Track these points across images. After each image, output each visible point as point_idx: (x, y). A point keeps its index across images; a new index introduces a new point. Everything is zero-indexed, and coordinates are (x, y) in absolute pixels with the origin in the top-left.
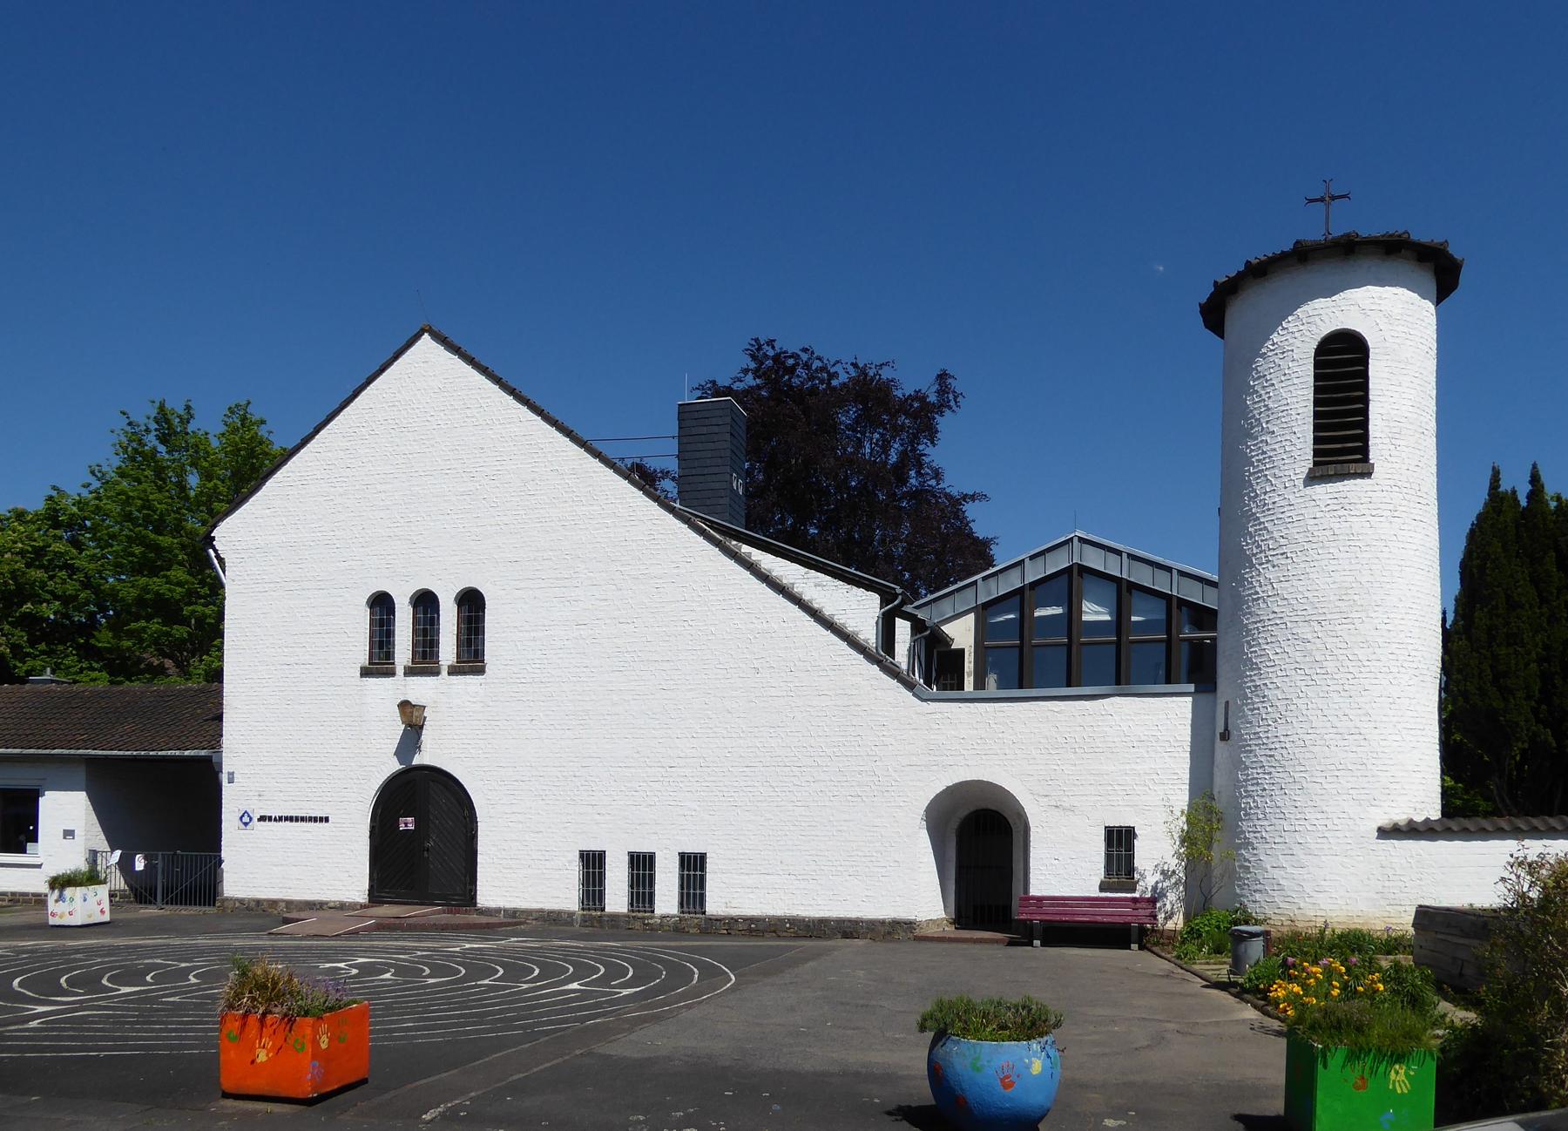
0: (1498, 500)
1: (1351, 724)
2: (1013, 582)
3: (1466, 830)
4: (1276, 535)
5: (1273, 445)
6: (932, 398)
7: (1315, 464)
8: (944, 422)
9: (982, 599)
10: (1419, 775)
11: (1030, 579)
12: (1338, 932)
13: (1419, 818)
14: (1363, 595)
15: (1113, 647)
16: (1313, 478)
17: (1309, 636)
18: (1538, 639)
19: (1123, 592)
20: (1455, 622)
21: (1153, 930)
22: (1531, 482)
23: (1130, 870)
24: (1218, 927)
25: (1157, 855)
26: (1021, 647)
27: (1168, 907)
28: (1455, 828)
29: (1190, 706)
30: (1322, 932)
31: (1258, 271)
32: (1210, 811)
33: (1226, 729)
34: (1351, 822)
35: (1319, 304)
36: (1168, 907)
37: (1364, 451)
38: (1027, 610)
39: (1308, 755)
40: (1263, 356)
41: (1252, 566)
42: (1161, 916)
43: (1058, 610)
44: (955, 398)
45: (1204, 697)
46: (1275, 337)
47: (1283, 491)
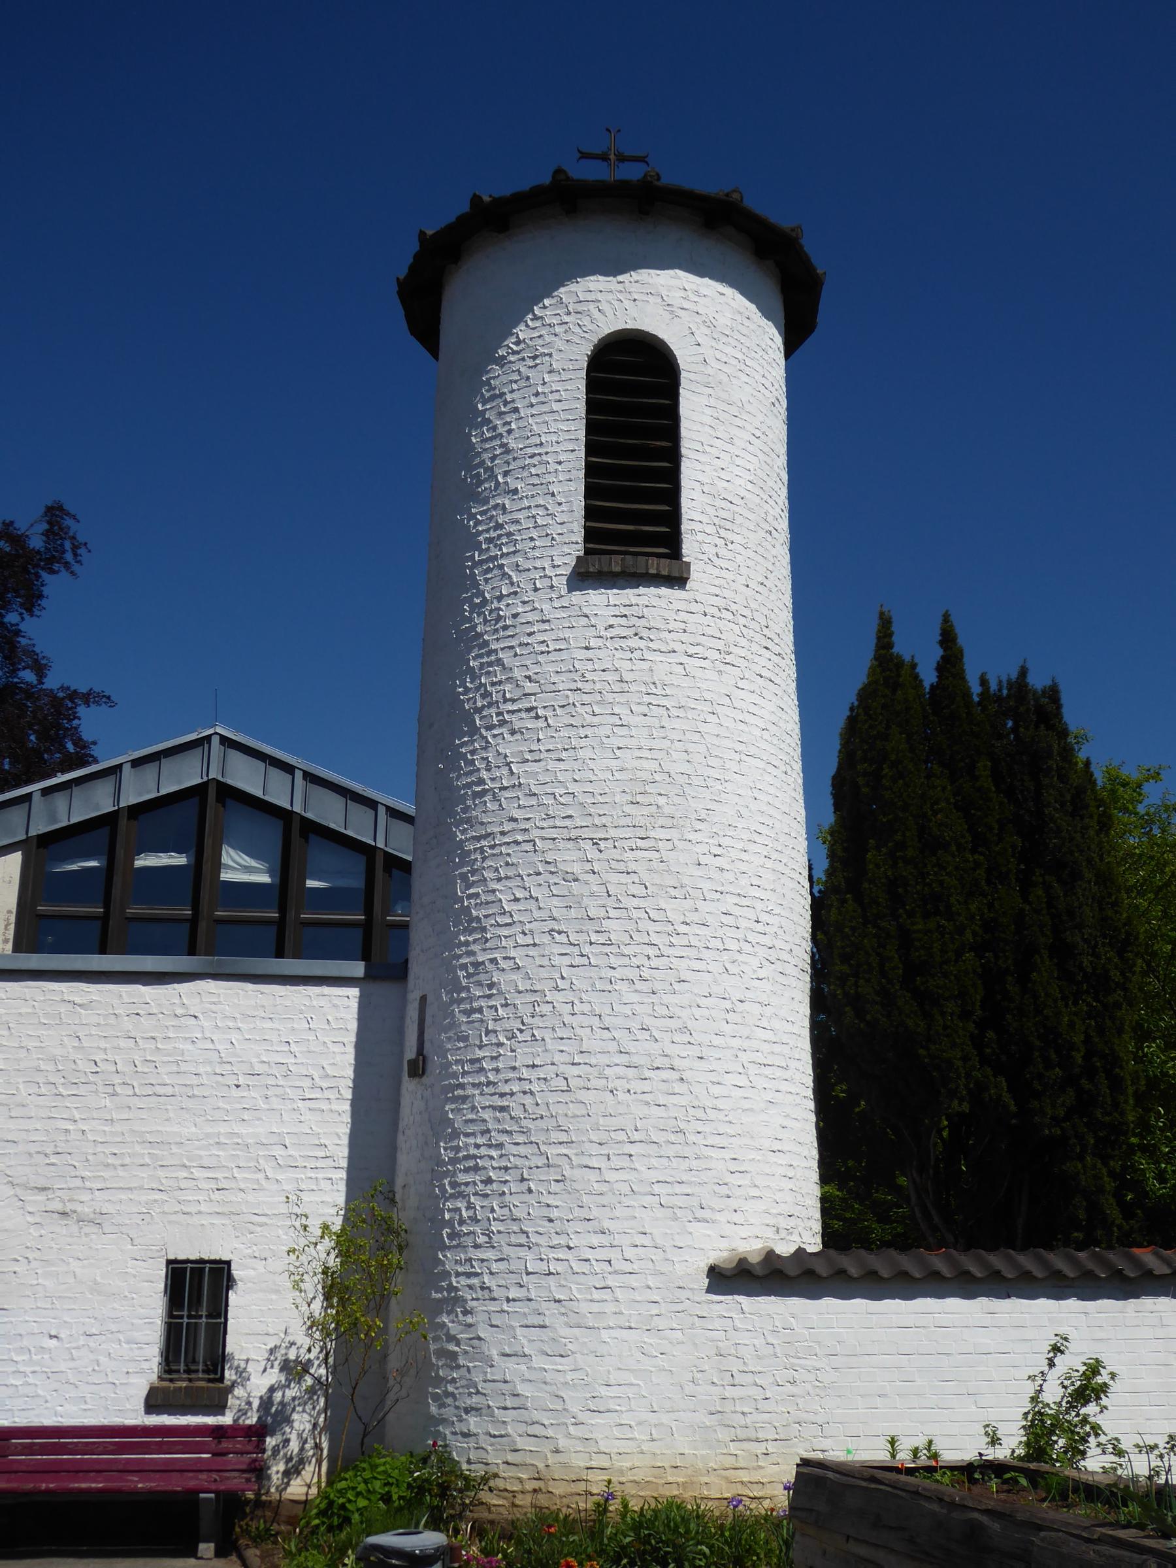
0: (889, 668)
1: (655, 1048)
2: (99, 801)
3: (904, 1276)
4: (517, 674)
5: (516, 513)
6: (36, 542)
7: (588, 552)
8: (54, 584)
9: (40, 827)
10: (782, 1159)
11: (131, 797)
12: (635, 1505)
13: (785, 1249)
14: (668, 788)
15: (273, 930)
16: (585, 576)
17: (576, 868)
18: (973, 907)
19: (294, 836)
20: (830, 873)
21: (258, 1504)
22: (941, 643)
23: (217, 1360)
24: (386, 1498)
25: (271, 1324)
26: (105, 918)
27: (294, 1446)
28: (853, 1271)
29: (354, 1005)
30: (602, 1509)
31: (493, 219)
32: (388, 1228)
33: (420, 1051)
34: (657, 1256)
35: (596, 283)
36: (294, 1446)
37: (671, 543)
38: (120, 853)
39: (573, 1109)
40: (501, 361)
41: (474, 731)
42: (277, 1469)
43: (179, 860)
44: (75, 548)
45: (384, 991)
46: (521, 332)
47: (531, 596)
